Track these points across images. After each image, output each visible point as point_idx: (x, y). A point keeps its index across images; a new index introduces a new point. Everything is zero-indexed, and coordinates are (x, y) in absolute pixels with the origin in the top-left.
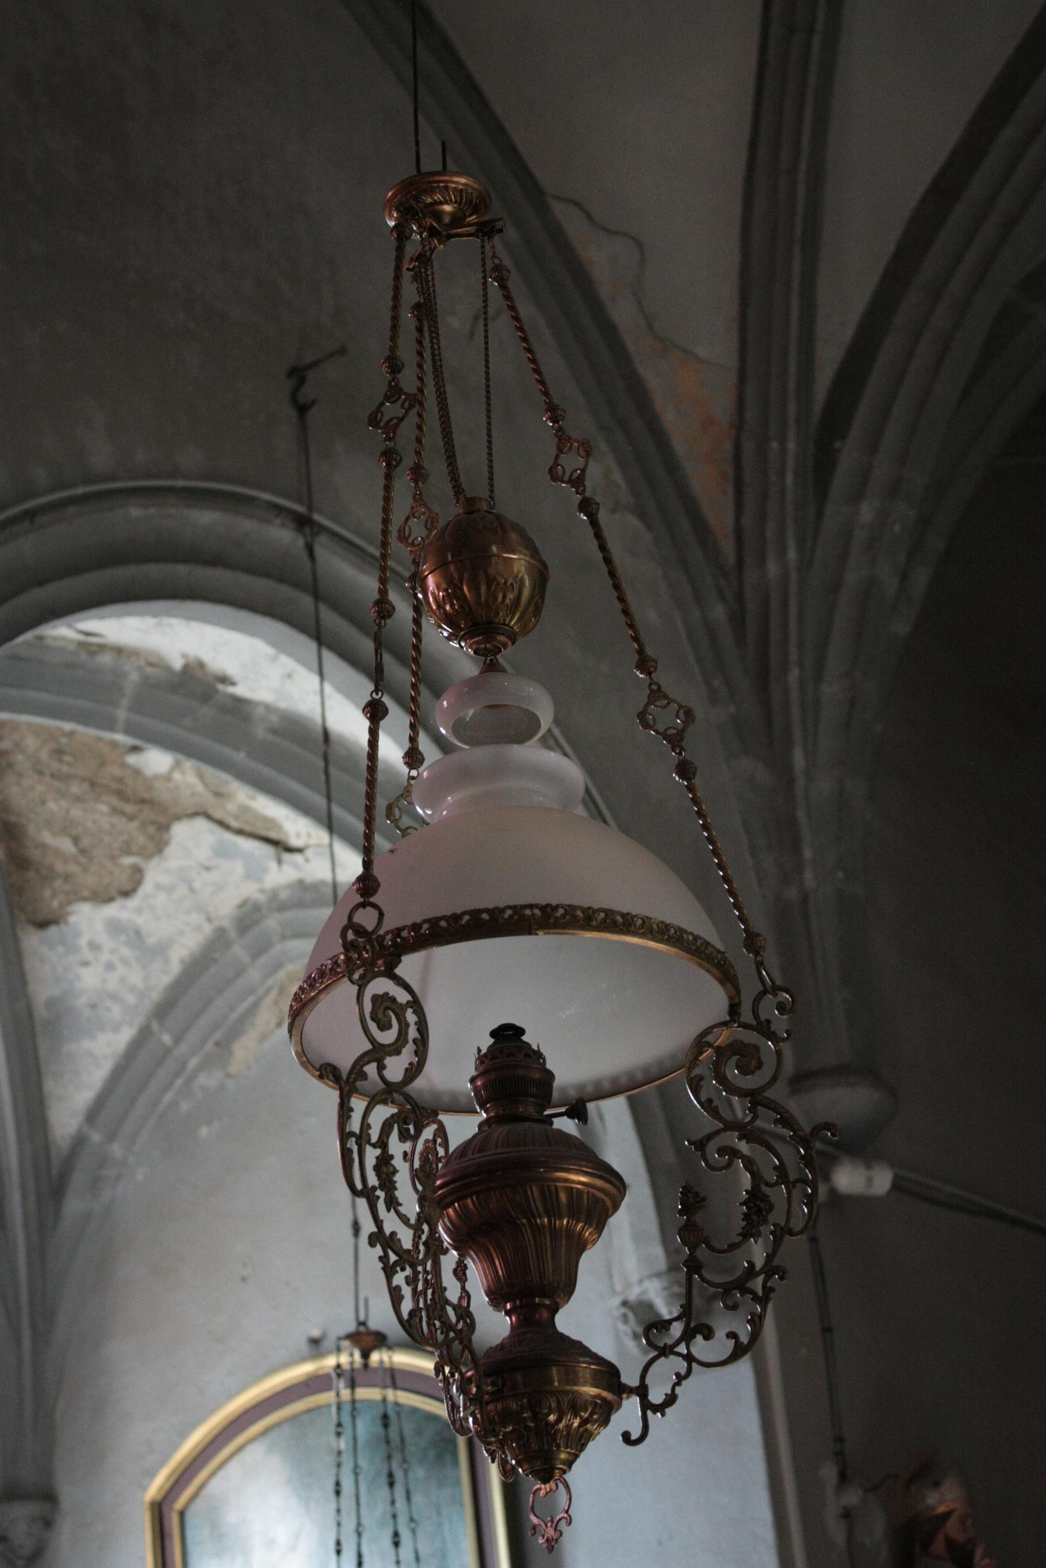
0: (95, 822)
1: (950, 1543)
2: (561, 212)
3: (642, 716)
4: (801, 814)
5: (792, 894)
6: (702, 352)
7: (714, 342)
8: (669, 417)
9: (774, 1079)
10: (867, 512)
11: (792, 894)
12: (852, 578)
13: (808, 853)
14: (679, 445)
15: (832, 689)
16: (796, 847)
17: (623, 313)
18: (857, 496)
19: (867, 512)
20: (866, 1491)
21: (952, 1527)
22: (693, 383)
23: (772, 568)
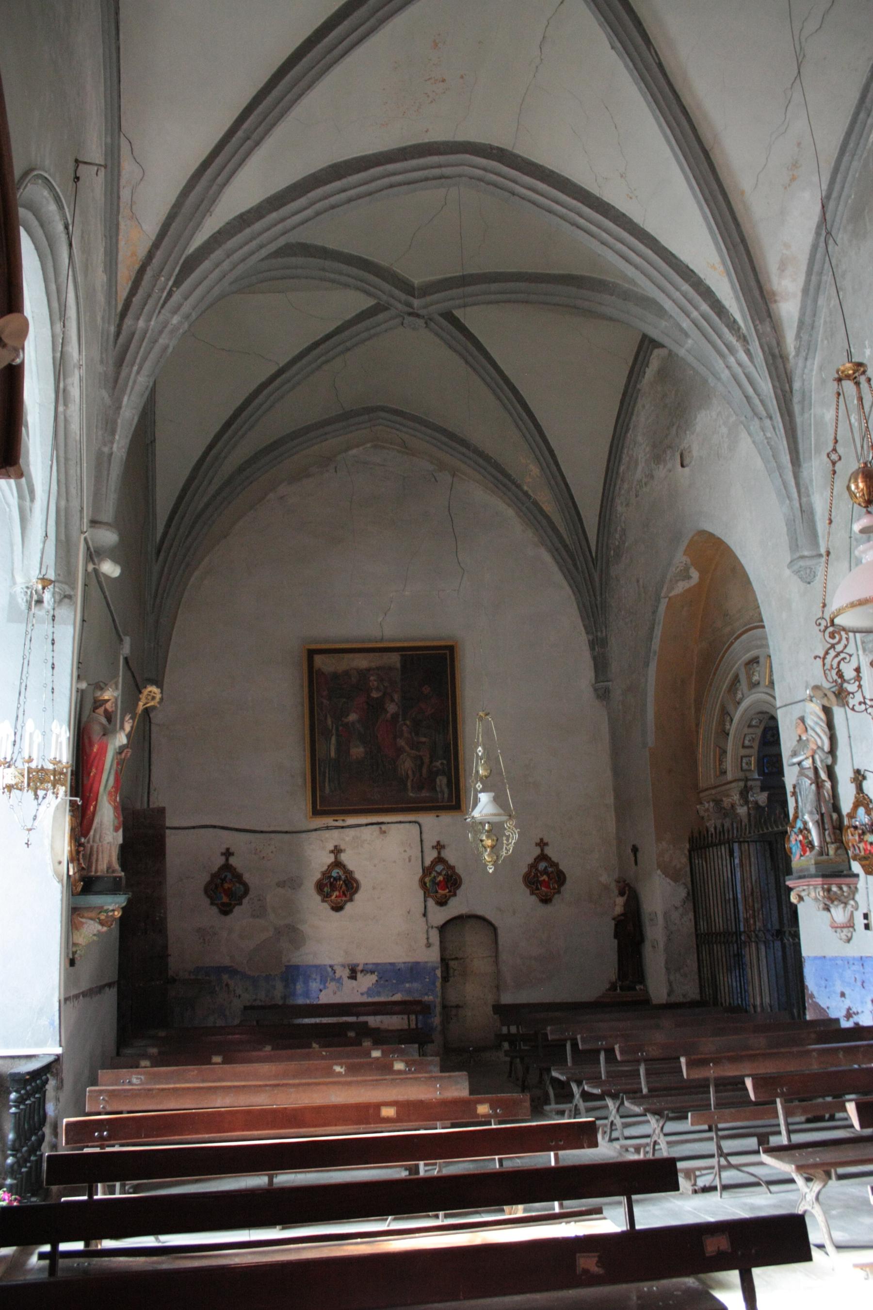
0: (644, 406)
1: (106, 711)
2: (124, 142)
3: (840, 459)
4: (119, 421)
5: (106, 450)
6: (145, 227)
7: (151, 227)
8: (122, 244)
9: (802, 557)
10: (175, 320)
11: (106, 450)
12: (161, 341)
13: (117, 437)
14: (120, 257)
15: (141, 379)
16: (113, 432)
17: (125, 194)
18: (175, 312)
19: (175, 320)
20: (89, 685)
21: (108, 706)
22: (138, 235)
23: (141, 323)
